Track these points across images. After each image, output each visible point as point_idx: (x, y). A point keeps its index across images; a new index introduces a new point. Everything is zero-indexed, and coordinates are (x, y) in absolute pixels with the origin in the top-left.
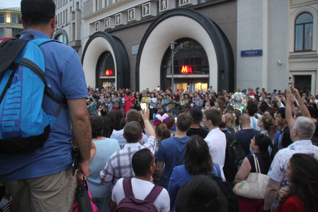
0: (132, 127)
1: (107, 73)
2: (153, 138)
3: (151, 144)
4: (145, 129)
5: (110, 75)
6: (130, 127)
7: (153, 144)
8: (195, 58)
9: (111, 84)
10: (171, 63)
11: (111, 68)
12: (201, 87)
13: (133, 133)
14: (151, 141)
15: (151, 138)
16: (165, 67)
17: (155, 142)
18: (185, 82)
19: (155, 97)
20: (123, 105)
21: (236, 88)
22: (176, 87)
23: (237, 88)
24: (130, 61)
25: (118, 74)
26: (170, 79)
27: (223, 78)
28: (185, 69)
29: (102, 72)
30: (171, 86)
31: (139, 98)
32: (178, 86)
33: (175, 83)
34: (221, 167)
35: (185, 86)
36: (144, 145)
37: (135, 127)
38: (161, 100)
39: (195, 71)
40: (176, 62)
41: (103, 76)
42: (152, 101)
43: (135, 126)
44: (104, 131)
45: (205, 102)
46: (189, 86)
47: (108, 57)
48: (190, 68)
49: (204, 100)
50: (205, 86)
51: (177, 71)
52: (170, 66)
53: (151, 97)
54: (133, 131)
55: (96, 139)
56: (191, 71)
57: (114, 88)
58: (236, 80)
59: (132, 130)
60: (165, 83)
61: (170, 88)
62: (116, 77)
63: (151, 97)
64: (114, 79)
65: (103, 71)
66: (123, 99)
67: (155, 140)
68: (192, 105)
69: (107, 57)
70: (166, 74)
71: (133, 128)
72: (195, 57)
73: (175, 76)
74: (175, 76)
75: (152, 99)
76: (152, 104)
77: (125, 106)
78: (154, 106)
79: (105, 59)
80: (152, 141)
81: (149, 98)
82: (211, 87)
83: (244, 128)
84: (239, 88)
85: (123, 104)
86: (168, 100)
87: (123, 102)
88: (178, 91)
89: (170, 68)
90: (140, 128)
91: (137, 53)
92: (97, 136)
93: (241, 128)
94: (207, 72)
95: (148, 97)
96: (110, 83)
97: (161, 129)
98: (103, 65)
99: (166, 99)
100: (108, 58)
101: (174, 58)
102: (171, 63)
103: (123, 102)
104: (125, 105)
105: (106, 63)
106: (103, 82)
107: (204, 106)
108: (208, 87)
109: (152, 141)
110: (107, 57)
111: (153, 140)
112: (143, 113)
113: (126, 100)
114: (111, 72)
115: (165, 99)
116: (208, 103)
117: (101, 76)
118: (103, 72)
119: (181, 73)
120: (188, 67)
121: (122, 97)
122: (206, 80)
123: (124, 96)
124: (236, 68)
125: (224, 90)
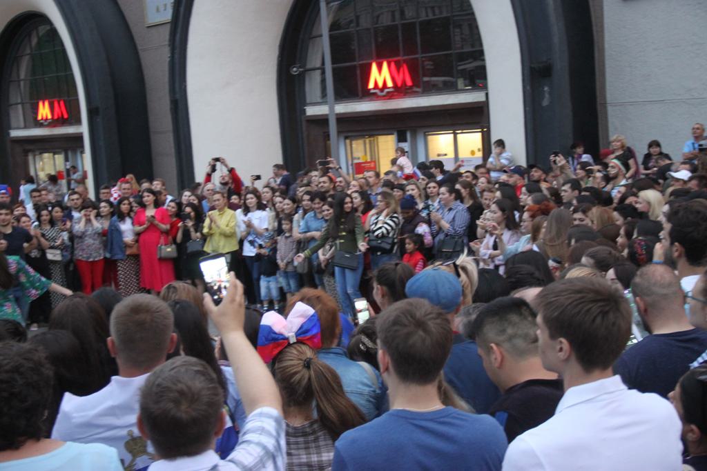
0: (180, 386)
1: (44, 111)
2: (270, 417)
3: (265, 448)
4: (227, 371)
5: (57, 122)
6: (168, 389)
7: (270, 443)
8: (427, 24)
9: (67, 160)
10: (321, 51)
11: (61, 90)
12: (454, 147)
13: (184, 416)
14: (262, 430)
15: (261, 415)
16: (295, 71)
17: (278, 434)
18: (386, 131)
19: (261, 207)
20: (128, 252)
21: (607, 136)
22: (349, 154)
23: (613, 137)
24: (142, 55)
25: (92, 113)
26: (322, 121)
27: (545, 103)
28: (380, 75)
29: (20, 107)
30: (327, 152)
31: (192, 214)
32: (359, 149)
33: (346, 138)
34: (486, 305)
35: (387, 145)
36: (232, 455)
37: (189, 388)
38: (290, 218)
39: (425, 75)
40: (341, 48)
41: (26, 127)
42: (249, 225)
43: (190, 383)
44: (49, 414)
45: (476, 211)
46: (406, 146)
47: (40, 39)
48: (405, 69)
49: (469, 203)
50: (471, 141)
51: (350, 83)
52: (318, 64)
53: (247, 210)
54: (183, 407)
55: (16, 453)
56: (409, 83)
57: (85, 176)
58: (604, 105)
59: (177, 402)
60: (302, 142)
61: (328, 163)
62: (84, 129)
63: (247, 210)
64: (78, 138)
65: (22, 104)
66: (127, 227)
67: (277, 421)
68: (422, 229)
69: (34, 41)
70: (305, 104)
71: (181, 393)
72: (423, 17)
73: (343, 108)
74: (343, 108)
75: (250, 215)
76: (250, 238)
77: (136, 257)
78: (261, 246)
79: (28, 51)
80: (269, 434)
81: (239, 211)
82: (501, 143)
83: (662, 329)
84: (622, 137)
85: (127, 246)
86: (320, 216)
87: (129, 238)
88: (359, 168)
89: (317, 76)
90: (215, 388)
91: (167, 16)
92: (23, 438)
93: (646, 327)
94: (478, 78)
95: (234, 207)
96: (60, 158)
97: (296, 373)
98: (22, 76)
99: (311, 214)
100: (38, 43)
101: (334, 26)
102: (321, 51)
103: (129, 238)
104: (134, 250)
105: (33, 71)
106: (26, 152)
107: (471, 233)
108: (487, 151)
109: (269, 434)
110: (34, 41)
111: (270, 425)
112: (217, 302)
113: (138, 228)
114: (61, 110)
115: (305, 212)
116: (490, 217)
117: (18, 128)
118: (23, 109)
119: (366, 94)
120: (393, 65)
121: (122, 217)
122: (475, 117)
123: (129, 215)
124: (602, 50)
125: (556, 154)
